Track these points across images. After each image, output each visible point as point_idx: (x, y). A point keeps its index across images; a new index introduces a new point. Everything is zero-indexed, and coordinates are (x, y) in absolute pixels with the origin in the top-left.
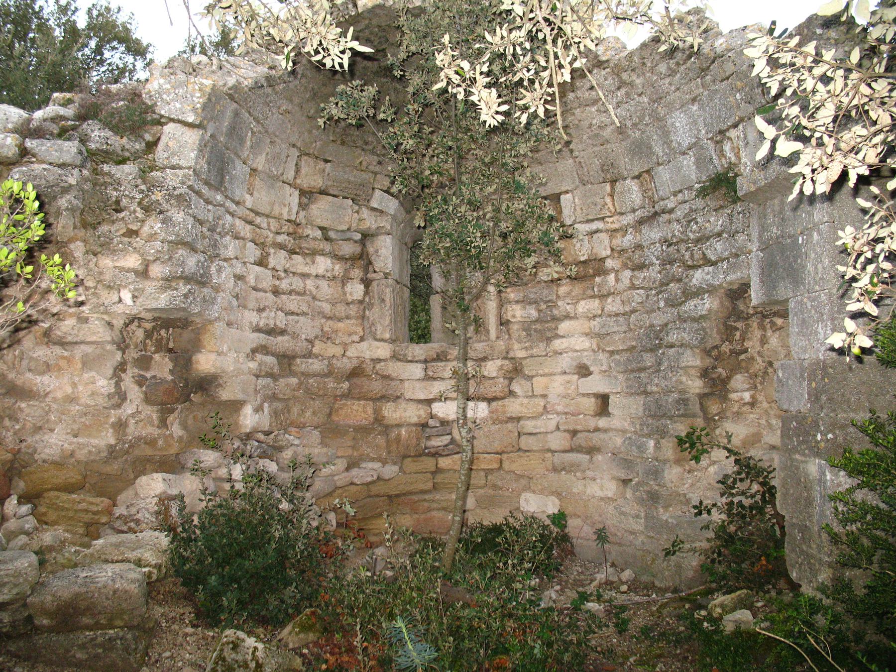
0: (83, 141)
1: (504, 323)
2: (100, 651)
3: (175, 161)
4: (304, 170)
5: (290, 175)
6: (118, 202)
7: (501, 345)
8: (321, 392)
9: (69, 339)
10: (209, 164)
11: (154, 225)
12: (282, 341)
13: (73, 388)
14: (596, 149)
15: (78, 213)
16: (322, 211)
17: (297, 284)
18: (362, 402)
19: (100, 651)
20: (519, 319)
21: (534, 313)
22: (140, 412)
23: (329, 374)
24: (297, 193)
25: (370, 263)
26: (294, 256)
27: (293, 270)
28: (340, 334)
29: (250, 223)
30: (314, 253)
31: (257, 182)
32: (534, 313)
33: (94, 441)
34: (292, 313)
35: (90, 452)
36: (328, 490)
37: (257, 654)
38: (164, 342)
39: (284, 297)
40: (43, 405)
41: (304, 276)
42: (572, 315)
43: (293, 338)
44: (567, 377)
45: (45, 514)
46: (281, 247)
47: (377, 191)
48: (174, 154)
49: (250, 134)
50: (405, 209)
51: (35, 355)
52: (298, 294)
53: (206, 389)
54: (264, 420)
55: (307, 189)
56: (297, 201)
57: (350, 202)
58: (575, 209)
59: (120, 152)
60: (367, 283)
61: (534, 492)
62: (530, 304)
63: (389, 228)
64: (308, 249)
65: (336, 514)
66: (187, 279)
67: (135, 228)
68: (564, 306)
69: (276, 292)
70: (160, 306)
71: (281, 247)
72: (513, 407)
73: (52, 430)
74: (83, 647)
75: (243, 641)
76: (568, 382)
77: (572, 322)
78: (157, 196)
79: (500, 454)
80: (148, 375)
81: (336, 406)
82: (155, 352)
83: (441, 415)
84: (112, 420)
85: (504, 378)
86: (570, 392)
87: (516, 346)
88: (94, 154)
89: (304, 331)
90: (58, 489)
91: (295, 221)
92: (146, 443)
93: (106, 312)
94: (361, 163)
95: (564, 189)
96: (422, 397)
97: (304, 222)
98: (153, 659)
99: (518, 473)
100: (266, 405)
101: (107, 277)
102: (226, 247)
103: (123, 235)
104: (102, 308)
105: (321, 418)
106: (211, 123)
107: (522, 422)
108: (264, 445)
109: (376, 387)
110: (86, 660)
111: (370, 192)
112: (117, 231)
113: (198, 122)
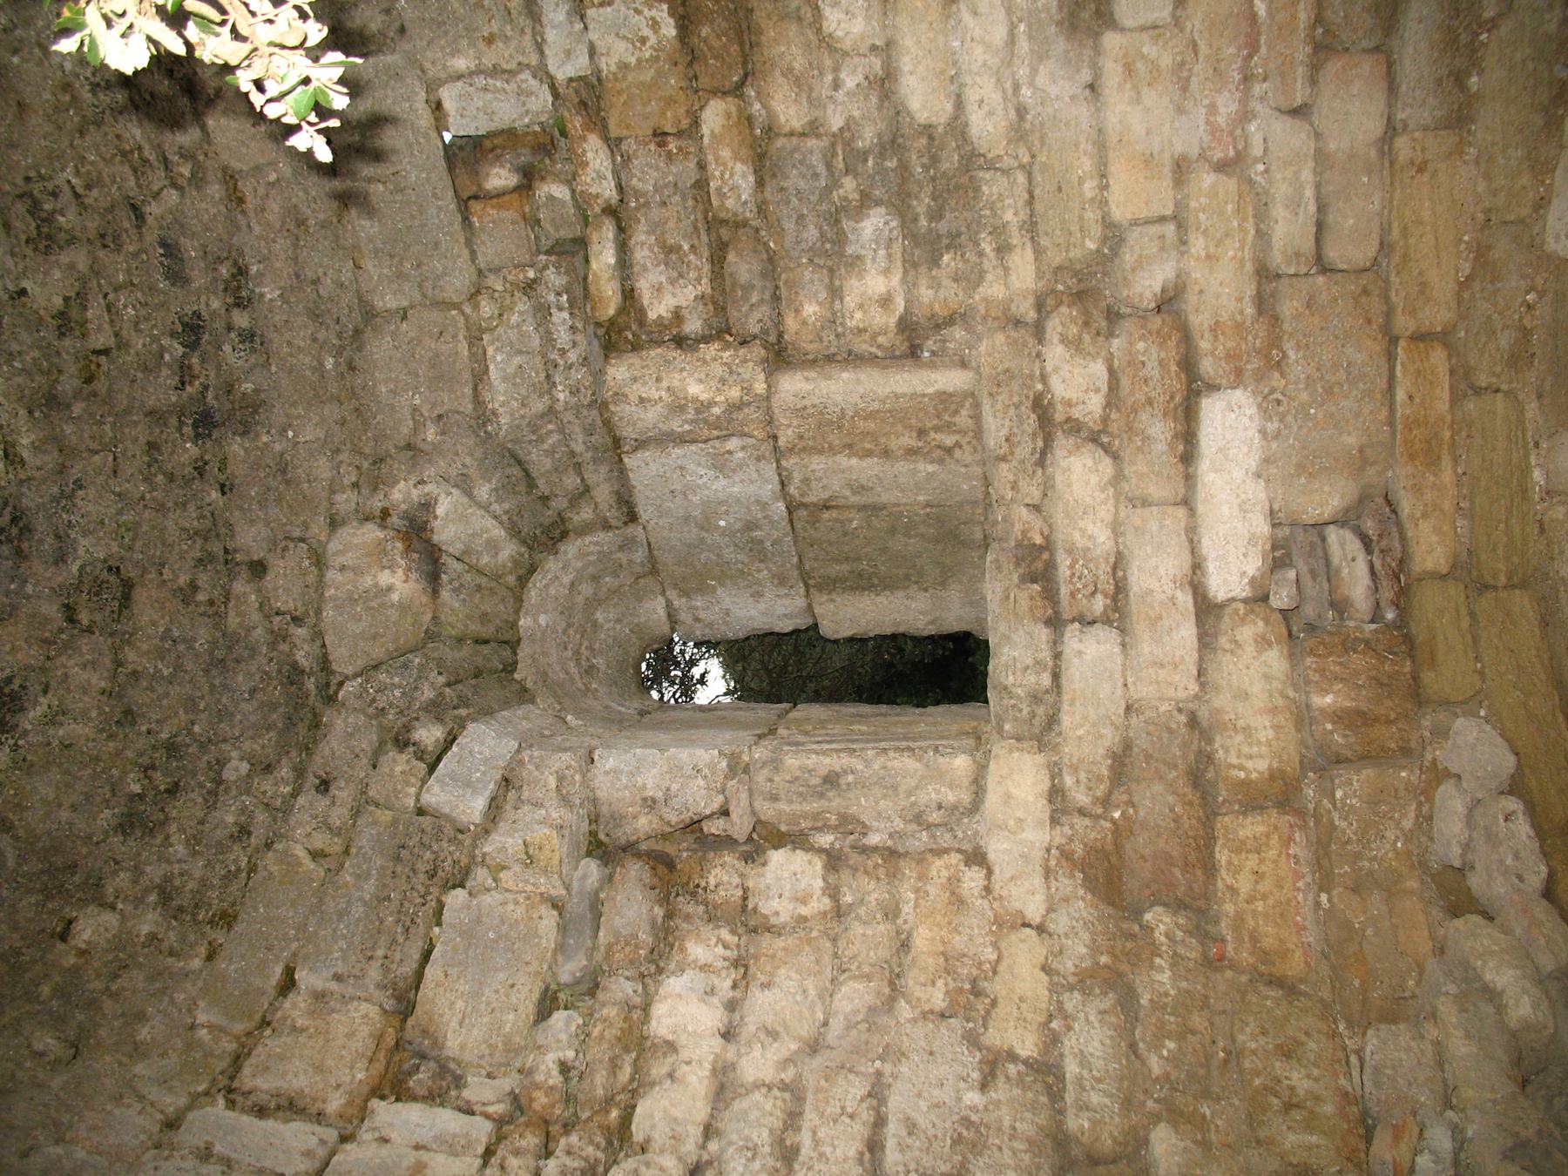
1: (913, 340)
4: (298, 1079)
7: (992, 349)
16: (472, 1011)
18: (1222, 856)
20: (896, 280)
21: (874, 225)
24: (385, 1112)
25: (693, 826)
26: (638, 1130)
27: (695, 1133)
28: (959, 942)
30: (636, 1041)
32: (874, 225)
41: (724, 1087)
42: (877, 64)
43: (978, 1147)
44: (1112, 72)
47: (428, 799)
50: (506, 704)
52: (793, 1119)
58: (496, 71)
60: (766, 838)
61: (1542, 204)
62: (840, 240)
63: (566, 757)
64: (614, 1067)
68: (846, 105)
72: (1220, 291)
76: (1129, 69)
77: (906, 63)
79: (1394, 341)
81: (1246, 958)
83: (1254, 565)
85: (1111, 334)
86: (1166, 61)
87: (993, 289)
91: (501, 1122)
94: (316, 855)
96: (1186, 633)
97: (508, 1083)
99: (1466, 268)
107: (1277, 260)
109: (1157, 802)
111: (426, 821)
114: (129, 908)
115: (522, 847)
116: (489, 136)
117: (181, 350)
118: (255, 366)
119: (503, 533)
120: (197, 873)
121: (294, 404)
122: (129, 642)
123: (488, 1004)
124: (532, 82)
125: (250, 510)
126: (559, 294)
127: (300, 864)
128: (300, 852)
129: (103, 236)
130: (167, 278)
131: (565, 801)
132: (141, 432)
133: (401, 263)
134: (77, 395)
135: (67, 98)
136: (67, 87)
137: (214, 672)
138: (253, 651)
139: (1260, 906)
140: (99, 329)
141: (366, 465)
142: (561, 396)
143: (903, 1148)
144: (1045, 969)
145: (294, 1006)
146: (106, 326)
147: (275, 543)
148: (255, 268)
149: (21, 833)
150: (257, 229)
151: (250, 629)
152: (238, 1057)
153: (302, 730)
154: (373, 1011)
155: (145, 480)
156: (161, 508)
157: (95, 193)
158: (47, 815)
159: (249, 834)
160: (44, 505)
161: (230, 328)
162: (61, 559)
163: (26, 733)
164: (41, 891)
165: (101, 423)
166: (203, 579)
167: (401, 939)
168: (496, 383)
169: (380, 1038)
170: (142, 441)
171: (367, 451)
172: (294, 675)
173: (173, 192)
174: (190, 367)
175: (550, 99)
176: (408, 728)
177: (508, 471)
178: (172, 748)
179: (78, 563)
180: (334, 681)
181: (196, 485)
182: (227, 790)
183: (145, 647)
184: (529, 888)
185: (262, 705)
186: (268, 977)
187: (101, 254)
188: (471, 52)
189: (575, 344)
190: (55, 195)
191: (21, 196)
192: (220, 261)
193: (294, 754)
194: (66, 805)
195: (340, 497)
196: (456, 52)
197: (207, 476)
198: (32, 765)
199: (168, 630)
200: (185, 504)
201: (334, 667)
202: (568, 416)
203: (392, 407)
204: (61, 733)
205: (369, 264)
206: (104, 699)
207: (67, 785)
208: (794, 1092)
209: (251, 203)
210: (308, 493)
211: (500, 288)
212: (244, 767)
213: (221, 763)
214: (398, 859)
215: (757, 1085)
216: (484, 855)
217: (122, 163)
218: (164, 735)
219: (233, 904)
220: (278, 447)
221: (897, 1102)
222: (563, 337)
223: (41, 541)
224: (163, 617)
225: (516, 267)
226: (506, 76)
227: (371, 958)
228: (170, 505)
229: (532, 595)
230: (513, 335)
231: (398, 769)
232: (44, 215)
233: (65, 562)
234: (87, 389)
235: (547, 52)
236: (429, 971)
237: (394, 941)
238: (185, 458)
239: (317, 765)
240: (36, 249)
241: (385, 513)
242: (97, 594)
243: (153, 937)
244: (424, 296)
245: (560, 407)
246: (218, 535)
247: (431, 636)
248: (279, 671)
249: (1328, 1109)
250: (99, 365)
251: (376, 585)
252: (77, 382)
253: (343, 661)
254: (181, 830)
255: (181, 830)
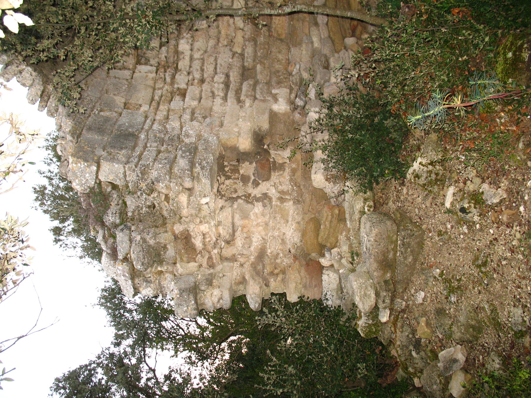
0: (116, 226)
2: (409, 250)
3: (121, 176)
5: (127, 73)
6: (149, 207)
8: (267, 47)
9: (231, 231)
10: (122, 148)
11: (161, 186)
12: (233, 77)
13: (260, 226)
15: (157, 230)
17: (197, 65)
19: (409, 250)
22: (275, 183)
23: (254, 40)
24: (139, 67)
26: (179, 67)
27: (188, 68)
28: (229, 32)
29: (159, 104)
30: (177, 52)
31: (133, 101)
33: (291, 212)
34: (216, 68)
35: (297, 214)
36: (330, 44)
37: (424, 163)
38: (233, 168)
39: (205, 76)
40: (269, 240)
41: (191, 59)
43: (231, 69)
45: (331, 244)
46: (173, 77)
48: (117, 176)
49: (102, 113)
51: (241, 245)
52: (203, 64)
53: (262, 137)
54: (282, 92)
55: (136, 60)
59: (120, 206)
64: (174, 57)
65: (346, 37)
66: (192, 164)
67: (164, 197)
69: (202, 81)
70: (210, 183)
71: (173, 77)
73: (284, 234)
74: (405, 258)
75: (415, 170)
78: (143, 185)
80: (253, 178)
81: (276, 35)
82: (239, 173)
84: (278, 203)
88: (123, 220)
89: (226, 60)
90: (318, 235)
91: (157, 67)
92: (294, 175)
93: (214, 212)
97: (157, 60)
98: (419, 220)
100: (274, 91)
101: (193, 212)
102: (173, 129)
103: (168, 202)
104: (212, 214)
105: (283, 47)
106: (97, 153)
108: (299, 94)
110: (413, 257)
112: (166, 207)
113: (96, 164)
139: (279, 26)
143: (220, 69)
144: (243, 37)
208: (203, 59)
215: (197, 59)
221: (219, 61)
249: (284, 61)
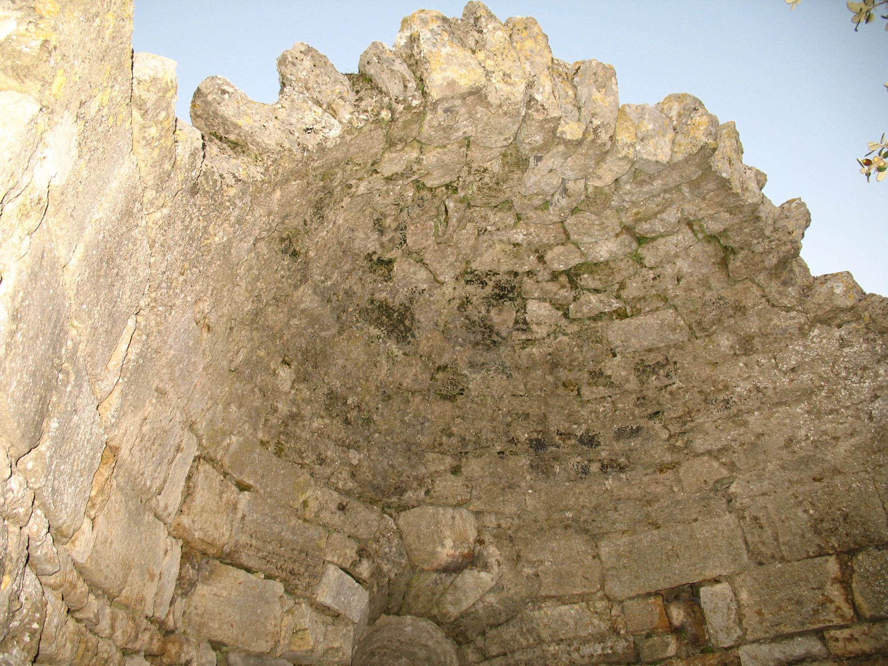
4: (201, 497)
14: (797, 488)
24: (177, 552)
56: (175, 570)
57: (278, 587)
94: (305, 504)
95: (709, 574)
114: (291, 397)
115: (303, 627)
116: (701, 609)
117: (579, 434)
118: (569, 474)
119: (464, 608)
120: (303, 435)
121: (547, 494)
122: (424, 399)
123: (224, 611)
124: (735, 636)
125: (490, 468)
126: (612, 648)
127: (302, 494)
128: (309, 493)
129: (644, 398)
130: (619, 429)
131: (326, 652)
132: (535, 410)
133: (627, 557)
134: (557, 378)
135: (720, 387)
136: (726, 387)
137: (404, 445)
138: (413, 467)
140: (592, 392)
141: (510, 532)
142: (552, 648)
145: (232, 492)
146: (594, 396)
147: (470, 481)
148: (624, 476)
149: (336, 339)
150: (646, 479)
151: (425, 465)
152: (212, 461)
153: (370, 494)
154: (225, 539)
155: (509, 411)
156: (493, 419)
157: (668, 396)
158: (342, 353)
159: (321, 465)
160: (500, 358)
161: (590, 461)
162: (472, 365)
163: (385, 343)
164: (307, 349)
165: (541, 390)
166: (454, 440)
167: (260, 554)
168: (558, 610)
169: (211, 544)
170: (530, 411)
171: (519, 534)
172: (400, 490)
173: (667, 436)
174: (569, 439)
175: (726, 646)
176: (369, 557)
177: (503, 614)
178: (368, 421)
179: (468, 374)
180: (392, 511)
181: (505, 439)
182: (344, 452)
183: (421, 408)
184: (283, 633)
185: (386, 471)
186: (249, 476)
187: (634, 396)
188: (752, 602)
189: (583, 657)
190: (667, 376)
191: (667, 359)
192: (628, 458)
193: (359, 490)
194: (346, 363)
195: (493, 517)
196: (750, 593)
197: (509, 444)
198: (369, 346)
199: (428, 420)
200: (494, 432)
201: (403, 513)
202: (538, 652)
203: (543, 549)
204: (384, 362)
205: (625, 539)
206: (397, 385)
207: (356, 364)
209: (660, 477)
210: (497, 500)
211: (613, 613)
212: (355, 462)
213: (358, 449)
214: (301, 552)
216: (300, 604)
217: (684, 411)
218: (375, 417)
219: (286, 456)
220: (523, 484)
222: (587, 650)
223: (482, 355)
224: (435, 418)
225: (625, 623)
226: (737, 620)
227: (251, 537)
228: (494, 424)
229: (423, 623)
230: (586, 620)
231: (348, 551)
232: (657, 369)
233: (470, 367)
234: (560, 384)
235: (754, 645)
236: (242, 572)
237: (259, 550)
238: (519, 433)
239: (355, 505)
240: (637, 364)
241: (481, 542)
242: (451, 383)
243: (276, 410)
244: (608, 570)
245: (545, 647)
246: (476, 449)
247: (413, 568)
248: (402, 482)
250: (572, 390)
251: (445, 537)
252: (564, 378)
253: (405, 518)
254: (326, 425)
255: (326, 425)
